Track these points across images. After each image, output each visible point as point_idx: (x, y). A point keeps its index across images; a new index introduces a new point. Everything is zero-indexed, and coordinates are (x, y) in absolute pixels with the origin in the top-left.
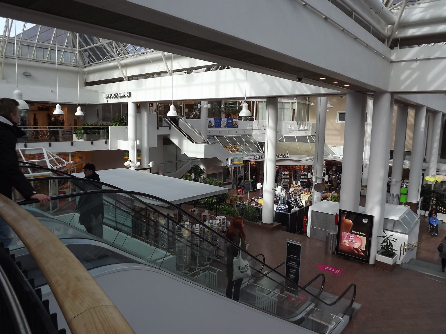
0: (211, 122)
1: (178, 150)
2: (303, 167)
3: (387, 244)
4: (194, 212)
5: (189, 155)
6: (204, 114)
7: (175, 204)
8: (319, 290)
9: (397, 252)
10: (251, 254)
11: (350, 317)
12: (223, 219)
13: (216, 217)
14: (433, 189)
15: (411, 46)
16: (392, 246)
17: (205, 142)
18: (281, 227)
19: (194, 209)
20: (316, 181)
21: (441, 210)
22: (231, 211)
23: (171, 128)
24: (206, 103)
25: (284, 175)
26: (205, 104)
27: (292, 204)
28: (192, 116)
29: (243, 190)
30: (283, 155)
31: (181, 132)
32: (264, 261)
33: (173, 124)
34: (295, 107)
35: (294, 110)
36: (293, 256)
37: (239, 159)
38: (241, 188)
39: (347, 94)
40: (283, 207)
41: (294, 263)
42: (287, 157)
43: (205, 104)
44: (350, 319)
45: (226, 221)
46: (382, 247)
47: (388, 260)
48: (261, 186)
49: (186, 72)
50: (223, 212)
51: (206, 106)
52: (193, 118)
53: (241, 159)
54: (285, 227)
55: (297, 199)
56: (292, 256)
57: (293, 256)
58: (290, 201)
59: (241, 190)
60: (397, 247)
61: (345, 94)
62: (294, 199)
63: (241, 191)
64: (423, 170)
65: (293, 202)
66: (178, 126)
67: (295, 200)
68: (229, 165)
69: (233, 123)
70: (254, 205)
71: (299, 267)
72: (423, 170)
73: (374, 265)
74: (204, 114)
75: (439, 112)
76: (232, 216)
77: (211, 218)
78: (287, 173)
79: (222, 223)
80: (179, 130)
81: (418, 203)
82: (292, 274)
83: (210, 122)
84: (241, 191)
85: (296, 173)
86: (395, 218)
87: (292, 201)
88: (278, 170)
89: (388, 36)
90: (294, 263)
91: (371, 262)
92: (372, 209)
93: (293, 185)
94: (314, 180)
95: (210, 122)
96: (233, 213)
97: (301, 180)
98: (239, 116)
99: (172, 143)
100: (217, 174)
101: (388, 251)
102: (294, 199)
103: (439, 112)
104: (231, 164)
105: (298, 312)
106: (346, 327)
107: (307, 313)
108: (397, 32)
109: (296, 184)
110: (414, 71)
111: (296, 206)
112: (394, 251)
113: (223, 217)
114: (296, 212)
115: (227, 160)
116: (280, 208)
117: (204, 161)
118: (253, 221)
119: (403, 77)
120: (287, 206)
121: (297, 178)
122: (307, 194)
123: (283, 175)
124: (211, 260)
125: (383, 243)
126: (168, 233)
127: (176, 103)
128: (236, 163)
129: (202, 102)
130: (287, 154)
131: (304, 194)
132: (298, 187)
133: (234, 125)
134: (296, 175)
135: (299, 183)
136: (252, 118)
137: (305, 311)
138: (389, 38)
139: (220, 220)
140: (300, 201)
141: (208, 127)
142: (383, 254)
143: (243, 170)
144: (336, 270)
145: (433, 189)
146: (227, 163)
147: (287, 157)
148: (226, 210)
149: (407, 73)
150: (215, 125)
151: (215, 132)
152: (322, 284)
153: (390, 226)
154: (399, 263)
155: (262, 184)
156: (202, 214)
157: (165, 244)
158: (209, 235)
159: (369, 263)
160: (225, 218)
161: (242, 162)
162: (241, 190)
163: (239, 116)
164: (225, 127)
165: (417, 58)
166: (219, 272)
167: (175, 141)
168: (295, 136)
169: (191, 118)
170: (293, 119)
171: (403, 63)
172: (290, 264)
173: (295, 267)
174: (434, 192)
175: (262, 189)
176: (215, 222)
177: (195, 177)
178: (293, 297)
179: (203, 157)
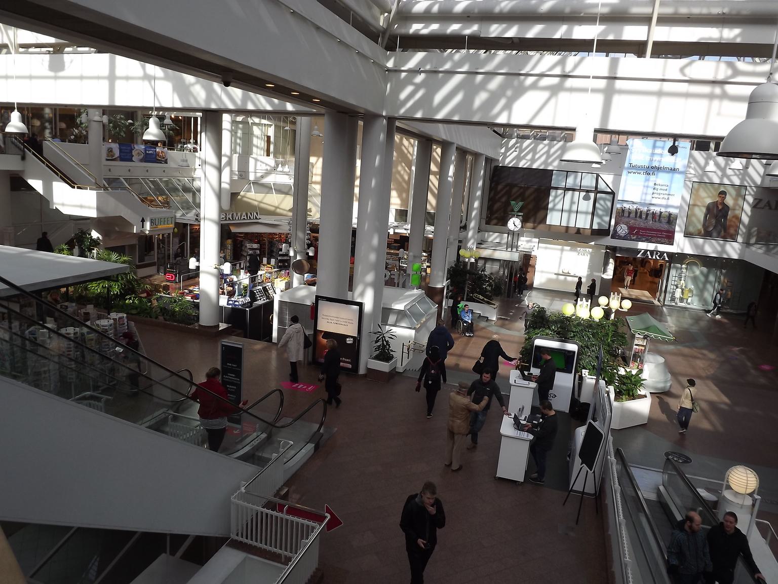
0: (111, 151)
1: (43, 202)
2: (286, 237)
3: (383, 344)
4: (67, 308)
5: (66, 211)
6: (95, 134)
7: (28, 290)
8: (275, 416)
9: (397, 355)
10: (183, 376)
11: (315, 447)
12: (120, 318)
13: (109, 314)
14: (469, 268)
15: (428, 49)
16: (389, 345)
17: (97, 186)
18: (233, 332)
19: (66, 304)
20: (295, 256)
21: (479, 298)
22: (146, 309)
23: (27, 157)
24: (97, 113)
25: (251, 249)
26: (96, 116)
27: (258, 296)
28: (72, 137)
29: (176, 276)
30: (249, 214)
31: (47, 166)
32: (192, 378)
33: (30, 151)
34: (271, 132)
35: (269, 138)
36: (230, 365)
37: (162, 220)
38: (172, 271)
39: (326, 115)
40: (241, 300)
41: (234, 375)
42: (256, 218)
43: (96, 116)
44: (317, 448)
45: (126, 320)
46: (376, 349)
47: (383, 366)
48: (197, 264)
49: (49, 51)
50: (130, 312)
51: (97, 118)
52: (75, 141)
53: (170, 219)
54: (240, 331)
55: (267, 287)
56: (230, 366)
57: (230, 365)
58: (255, 291)
59: (172, 276)
60: (396, 349)
61: (323, 115)
62: (261, 287)
63: (172, 278)
64: (460, 241)
65: (259, 292)
66: (42, 156)
67: (265, 289)
68: (146, 230)
69: (157, 154)
70: (190, 298)
71: (240, 381)
72: (460, 241)
73: (365, 376)
74: (95, 134)
75: (481, 155)
76: (146, 317)
77: (100, 317)
78: (255, 246)
79: (118, 325)
80: (43, 163)
81: (443, 288)
82: (231, 393)
83: (110, 151)
84: (172, 278)
85: (271, 246)
86: (400, 306)
87: (258, 291)
88: (225, 233)
89: (382, 29)
90: (234, 375)
91: (362, 371)
92: (362, 294)
93: (263, 265)
94: (292, 254)
95: (110, 151)
96: (149, 311)
97: (279, 258)
98: (143, 138)
99: (31, 189)
100: (127, 248)
101: (384, 354)
102: (261, 287)
103: (482, 154)
104: (150, 228)
105: (240, 446)
106: (308, 460)
107: (253, 448)
108: (396, 26)
109: (269, 263)
110: (418, 87)
111: (265, 298)
112: (391, 353)
113: (121, 315)
114: (260, 306)
115: (143, 221)
116: (235, 301)
117: (100, 223)
118: (186, 324)
119: (403, 96)
120: (249, 298)
121: (274, 255)
122: (285, 278)
123: (249, 249)
124: (100, 389)
125: (377, 342)
126: (11, 338)
127: (22, 108)
128: (160, 227)
129: (90, 111)
130: (255, 214)
131: (279, 279)
132: (271, 268)
133: (160, 159)
134: (272, 249)
135: (273, 261)
136: (194, 148)
137: (249, 445)
138: (384, 32)
139: (115, 320)
140: (272, 291)
141: (107, 160)
142: (377, 358)
143: (177, 240)
144: (308, 387)
145: (469, 268)
146: (143, 227)
147: (256, 218)
148: (136, 308)
149: (409, 89)
150: (120, 156)
151: (120, 169)
152: (279, 405)
153: (392, 319)
154: (400, 369)
155: (198, 260)
156: (83, 311)
157: (7, 364)
158: (93, 345)
159: (357, 373)
160: (125, 315)
161: (172, 226)
162: (172, 276)
163: (143, 138)
164: (141, 161)
165: (420, 69)
166: (107, 400)
167: (37, 184)
168: (272, 184)
169: (70, 141)
170: (268, 155)
171: (441, 75)
172: (227, 378)
173: (234, 381)
174: (470, 272)
175: (198, 268)
176: (104, 322)
177: (81, 253)
178: (236, 429)
179: (93, 214)
